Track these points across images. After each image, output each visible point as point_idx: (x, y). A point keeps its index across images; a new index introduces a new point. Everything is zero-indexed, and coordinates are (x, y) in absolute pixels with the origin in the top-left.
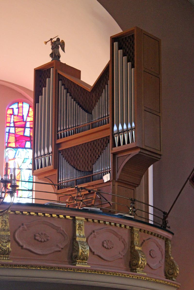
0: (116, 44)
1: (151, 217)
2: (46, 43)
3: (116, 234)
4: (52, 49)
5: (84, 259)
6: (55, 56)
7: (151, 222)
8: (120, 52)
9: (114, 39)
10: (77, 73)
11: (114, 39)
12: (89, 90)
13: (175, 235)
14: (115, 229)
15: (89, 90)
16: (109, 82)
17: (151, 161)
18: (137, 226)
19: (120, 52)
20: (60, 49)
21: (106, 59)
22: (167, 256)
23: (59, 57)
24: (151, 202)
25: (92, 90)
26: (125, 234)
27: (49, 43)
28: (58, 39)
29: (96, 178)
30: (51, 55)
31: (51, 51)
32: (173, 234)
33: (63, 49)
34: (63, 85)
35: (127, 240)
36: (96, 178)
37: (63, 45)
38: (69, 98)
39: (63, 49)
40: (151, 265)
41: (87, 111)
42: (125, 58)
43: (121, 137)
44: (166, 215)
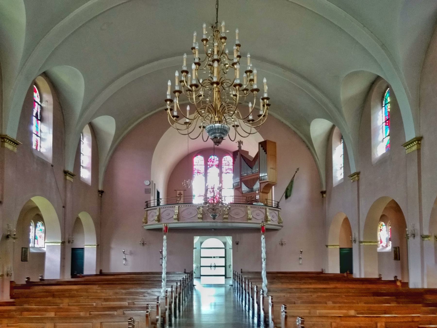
0: (260, 145)
1: (273, 204)
2: (236, 143)
3: (261, 211)
4: (239, 144)
5: (269, 221)
6: (240, 147)
7: (273, 206)
8: (262, 148)
9: (260, 143)
10: (247, 152)
11: (260, 143)
12: (251, 160)
13: (282, 209)
14: (260, 209)
15: (251, 160)
16: (258, 158)
17: (274, 185)
18: (268, 208)
19: (262, 148)
20: (241, 145)
21: (257, 150)
22: (279, 216)
23: (241, 147)
24: (273, 199)
25: (253, 160)
26: (264, 211)
27: (238, 142)
28: (241, 141)
29: (263, 170)
30: (238, 147)
31: (238, 145)
32: (280, 209)
33: (242, 144)
34: (243, 158)
35: (265, 213)
36: (263, 170)
37: (242, 143)
38: (245, 163)
39: (242, 144)
40: (273, 220)
41: (251, 168)
42: (264, 150)
43: (263, 178)
44: (278, 202)
